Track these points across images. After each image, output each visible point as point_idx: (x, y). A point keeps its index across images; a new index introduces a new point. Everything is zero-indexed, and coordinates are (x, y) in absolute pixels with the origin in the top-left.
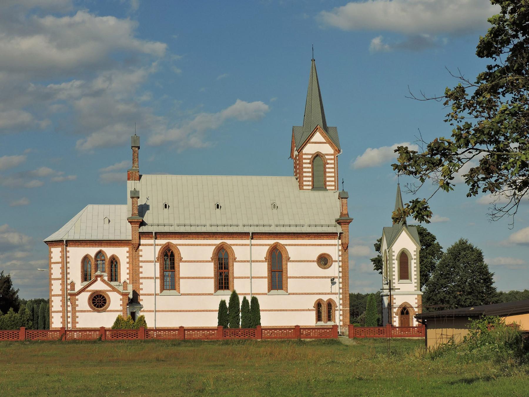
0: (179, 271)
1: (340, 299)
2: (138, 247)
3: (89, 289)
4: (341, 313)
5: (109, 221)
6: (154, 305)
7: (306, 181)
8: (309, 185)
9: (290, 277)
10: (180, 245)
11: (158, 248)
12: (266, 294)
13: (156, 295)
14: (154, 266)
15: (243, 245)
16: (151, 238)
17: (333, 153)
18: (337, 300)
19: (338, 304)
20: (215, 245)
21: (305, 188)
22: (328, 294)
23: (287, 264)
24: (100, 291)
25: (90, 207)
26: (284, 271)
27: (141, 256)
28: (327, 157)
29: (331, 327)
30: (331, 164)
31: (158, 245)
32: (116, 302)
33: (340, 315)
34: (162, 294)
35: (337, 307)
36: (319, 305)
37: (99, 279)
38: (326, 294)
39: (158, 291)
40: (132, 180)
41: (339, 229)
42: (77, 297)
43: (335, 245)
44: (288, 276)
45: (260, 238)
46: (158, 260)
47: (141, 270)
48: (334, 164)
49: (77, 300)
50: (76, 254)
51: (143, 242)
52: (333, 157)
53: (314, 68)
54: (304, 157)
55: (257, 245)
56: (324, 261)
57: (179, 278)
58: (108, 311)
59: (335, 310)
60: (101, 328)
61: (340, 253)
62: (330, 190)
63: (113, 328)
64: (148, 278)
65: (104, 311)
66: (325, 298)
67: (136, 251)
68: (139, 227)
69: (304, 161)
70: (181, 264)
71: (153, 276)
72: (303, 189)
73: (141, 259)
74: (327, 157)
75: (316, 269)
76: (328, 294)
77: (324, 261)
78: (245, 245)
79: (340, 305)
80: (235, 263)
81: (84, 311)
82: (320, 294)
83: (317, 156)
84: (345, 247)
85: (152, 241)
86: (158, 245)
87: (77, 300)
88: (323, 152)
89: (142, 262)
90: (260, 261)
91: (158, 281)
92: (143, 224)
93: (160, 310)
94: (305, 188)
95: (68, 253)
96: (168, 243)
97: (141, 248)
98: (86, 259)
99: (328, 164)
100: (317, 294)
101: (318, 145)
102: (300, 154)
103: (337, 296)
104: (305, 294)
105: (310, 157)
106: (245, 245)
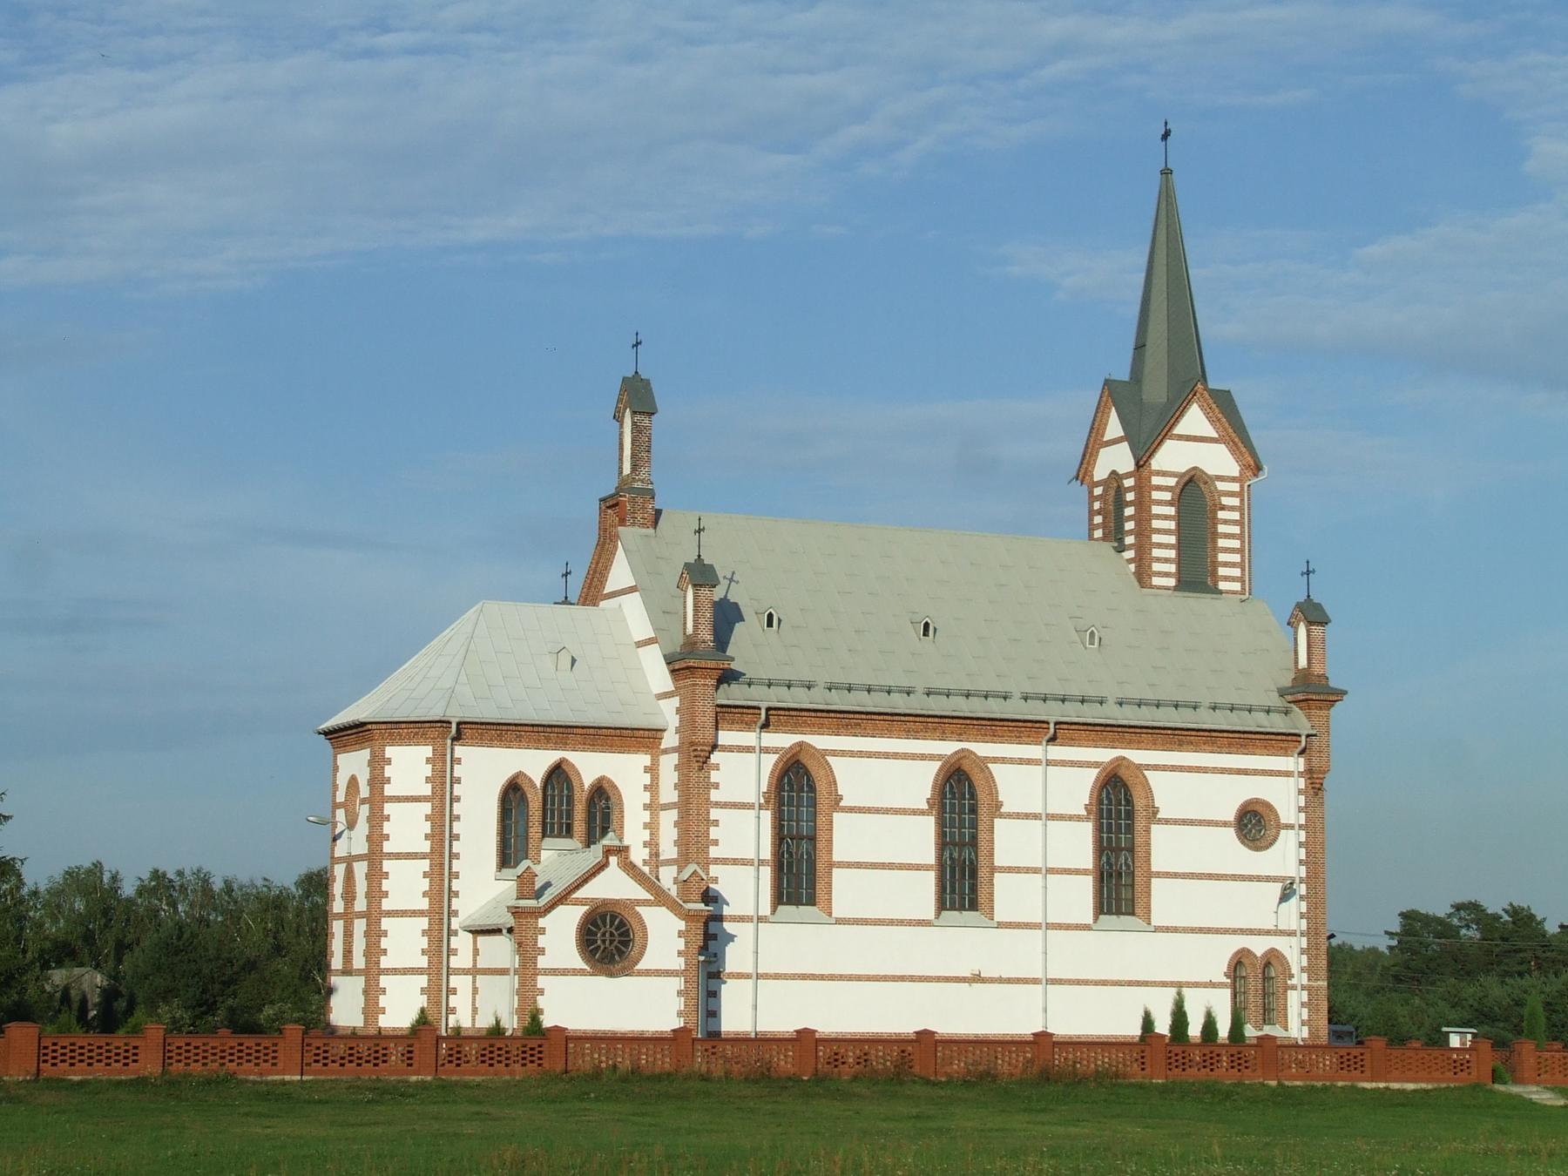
0: (830, 841)
1: (1303, 952)
2: (711, 752)
3: (579, 894)
4: (1305, 996)
5: (574, 661)
6: (1040, 957)
7: (1159, 560)
8: (1167, 575)
9: (1159, 875)
10: (834, 753)
11: (770, 761)
12: (1087, 927)
13: (760, 919)
14: (754, 821)
15: (1021, 761)
16: (748, 726)
18: (1293, 952)
19: (1295, 970)
20: (1095, 765)
21: (1156, 581)
22: (1268, 933)
23: (1148, 831)
24: (616, 902)
25: (493, 607)
27: (716, 786)
28: (1221, 486)
29: (913, 1037)
30: (1232, 508)
31: (767, 750)
32: (665, 939)
33: (1303, 1004)
34: (941, 921)
35: (1291, 976)
36: (1238, 963)
37: (613, 860)
38: (1259, 932)
39: (765, 909)
40: (633, 524)
41: (1300, 722)
42: (542, 922)
43: (1288, 774)
44: (1154, 869)
45: (1071, 742)
46: (767, 802)
47: (714, 833)
48: (1240, 509)
49: (543, 931)
50: (484, 772)
51: (726, 737)
52: (1235, 487)
53: (1167, 197)
54: (1156, 480)
55: (1063, 763)
56: (1254, 824)
57: (831, 865)
58: (641, 973)
59: (1287, 988)
60: (798, 1032)
61: (1302, 801)
62: (1227, 592)
64: (735, 862)
65: (627, 971)
66: (1259, 946)
67: (701, 768)
68: (717, 688)
70: (999, 823)
71: (751, 855)
72: (1152, 587)
73: (715, 796)
74: (1221, 486)
75: (1228, 850)
76: (1268, 933)
77: (1254, 824)
78: (1029, 762)
79: (1303, 970)
80: (1154, 828)
81: (564, 972)
82: (1243, 932)
83: (1191, 480)
84: (1315, 784)
85: (748, 738)
86: (767, 750)
87: (543, 931)
88: (1211, 471)
89: (718, 805)
90: (1071, 818)
91: (767, 873)
92: (728, 677)
93: (772, 971)
94: (1156, 581)
95: (456, 767)
96: (801, 744)
97: (716, 757)
98: (513, 792)
99: (1223, 508)
100: (1235, 932)
101: (1194, 447)
102: (1145, 472)
103: (1293, 940)
104: (1201, 930)
105: (1172, 482)
106: (1029, 762)
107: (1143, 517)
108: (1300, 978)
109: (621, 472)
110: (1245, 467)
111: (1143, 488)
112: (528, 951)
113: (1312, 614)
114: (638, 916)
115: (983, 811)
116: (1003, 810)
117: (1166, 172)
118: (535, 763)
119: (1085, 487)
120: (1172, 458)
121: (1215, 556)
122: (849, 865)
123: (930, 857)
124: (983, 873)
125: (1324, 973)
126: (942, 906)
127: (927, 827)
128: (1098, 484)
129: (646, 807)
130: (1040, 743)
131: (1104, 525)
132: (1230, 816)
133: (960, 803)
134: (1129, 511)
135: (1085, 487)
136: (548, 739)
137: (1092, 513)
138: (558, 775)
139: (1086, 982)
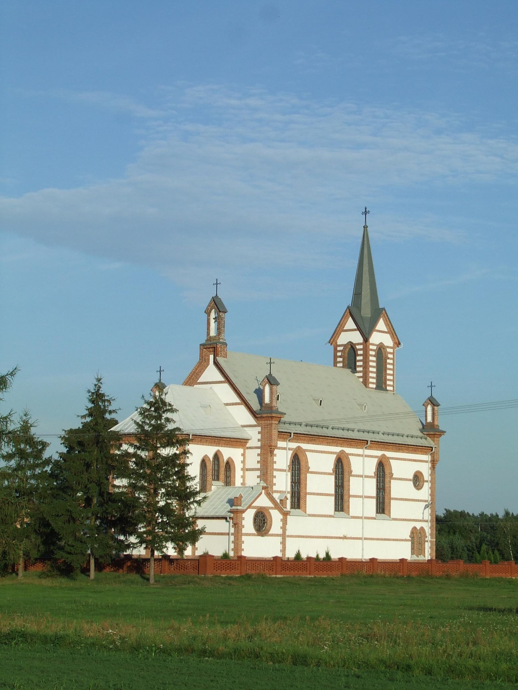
0: (306, 484)
3: (253, 505)
17: (392, 346)
22: (420, 521)
23: (390, 482)
26: (387, 490)
31: (289, 449)
35: (426, 537)
41: (429, 442)
44: (308, 491)
46: (289, 469)
56: (417, 480)
59: (425, 541)
63: (95, 578)
66: (418, 525)
69: (388, 361)
77: (417, 480)
84: (433, 463)
86: (289, 449)
88: (386, 345)
107: (366, 361)
108: (429, 538)
109: (208, 333)
110: (395, 343)
111: (366, 350)
112: (237, 526)
113: (433, 402)
114: (270, 513)
115: (346, 474)
116: (353, 473)
117: (365, 227)
118: (210, 451)
119: (332, 346)
120: (376, 338)
121: (386, 377)
122: (314, 494)
123: (333, 492)
124: (345, 497)
125: (434, 536)
126: (336, 510)
127: (332, 479)
128: (340, 346)
129: (242, 469)
130: (363, 448)
131: (343, 362)
132: (411, 477)
133: (341, 470)
134: (339, 354)
135: (332, 346)
136: (201, 441)
137: (335, 357)
138: (217, 456)
139: (394, 540)
